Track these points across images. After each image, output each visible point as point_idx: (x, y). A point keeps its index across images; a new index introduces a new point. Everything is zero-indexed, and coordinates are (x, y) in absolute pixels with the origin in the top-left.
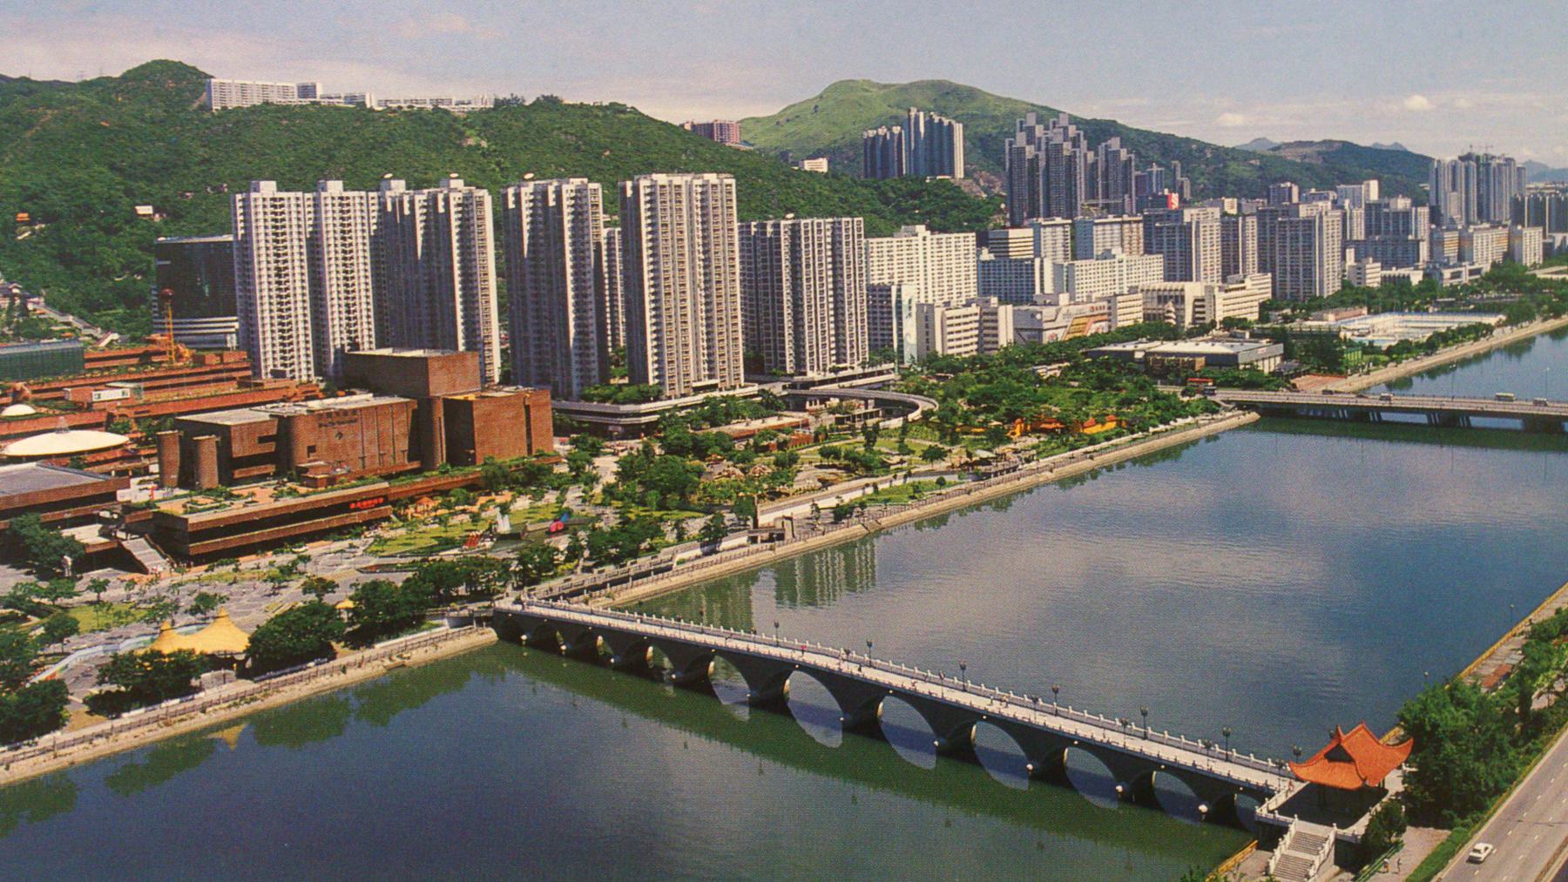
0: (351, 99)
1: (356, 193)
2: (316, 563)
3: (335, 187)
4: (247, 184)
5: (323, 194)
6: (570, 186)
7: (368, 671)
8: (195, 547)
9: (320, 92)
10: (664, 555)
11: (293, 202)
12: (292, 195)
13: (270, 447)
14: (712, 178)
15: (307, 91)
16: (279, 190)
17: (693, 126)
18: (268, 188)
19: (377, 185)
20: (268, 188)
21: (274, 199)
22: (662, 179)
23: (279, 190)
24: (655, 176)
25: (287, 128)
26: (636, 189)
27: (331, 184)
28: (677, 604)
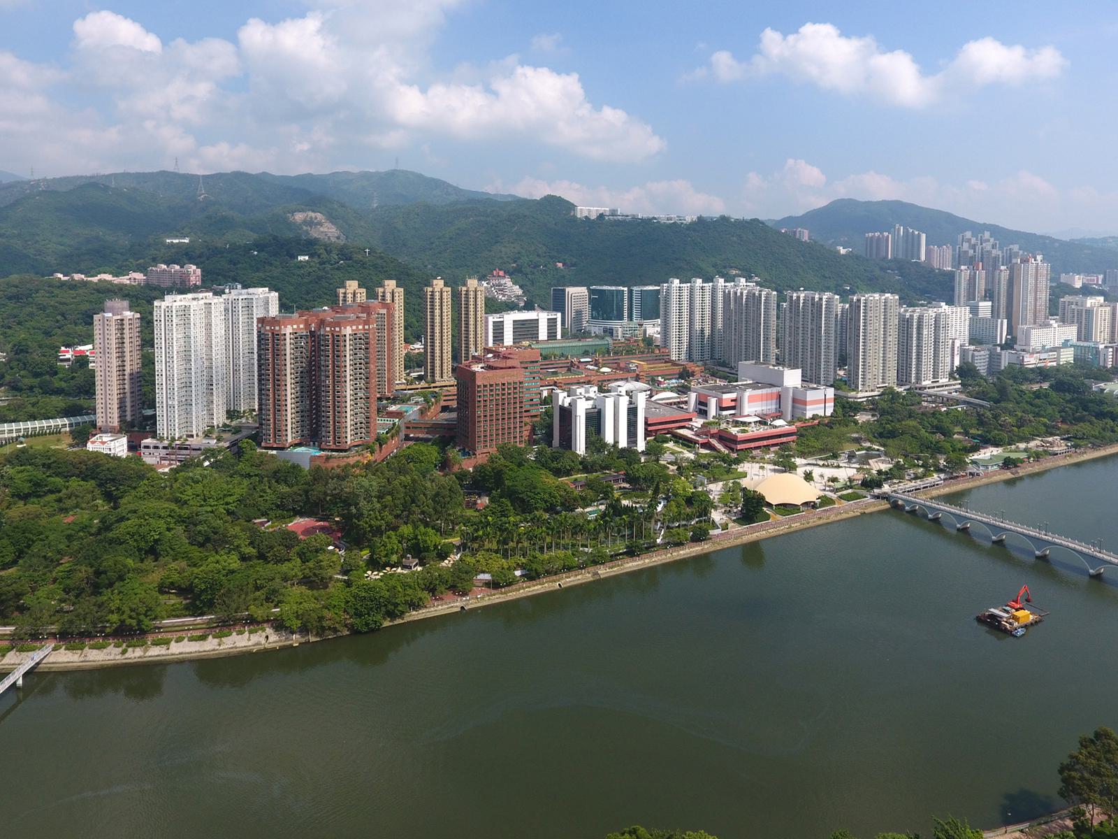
8: (739, 447)
26: (859, 300)
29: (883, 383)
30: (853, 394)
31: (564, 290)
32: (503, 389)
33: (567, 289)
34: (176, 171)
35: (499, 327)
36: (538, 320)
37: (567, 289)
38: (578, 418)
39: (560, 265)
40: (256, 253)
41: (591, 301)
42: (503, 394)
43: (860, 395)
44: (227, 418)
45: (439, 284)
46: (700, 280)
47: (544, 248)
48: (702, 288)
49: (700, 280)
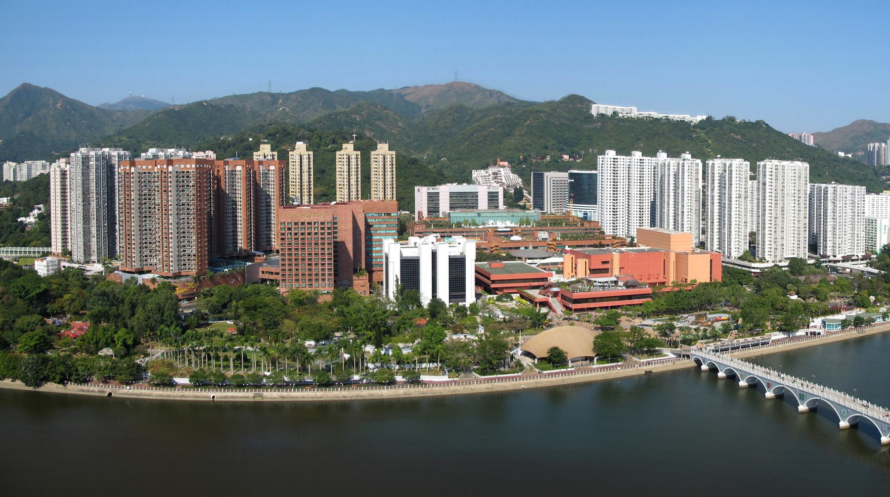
3: (638, 155)
20: (611, 154)
35: (433, 199)
37: (546, 174)
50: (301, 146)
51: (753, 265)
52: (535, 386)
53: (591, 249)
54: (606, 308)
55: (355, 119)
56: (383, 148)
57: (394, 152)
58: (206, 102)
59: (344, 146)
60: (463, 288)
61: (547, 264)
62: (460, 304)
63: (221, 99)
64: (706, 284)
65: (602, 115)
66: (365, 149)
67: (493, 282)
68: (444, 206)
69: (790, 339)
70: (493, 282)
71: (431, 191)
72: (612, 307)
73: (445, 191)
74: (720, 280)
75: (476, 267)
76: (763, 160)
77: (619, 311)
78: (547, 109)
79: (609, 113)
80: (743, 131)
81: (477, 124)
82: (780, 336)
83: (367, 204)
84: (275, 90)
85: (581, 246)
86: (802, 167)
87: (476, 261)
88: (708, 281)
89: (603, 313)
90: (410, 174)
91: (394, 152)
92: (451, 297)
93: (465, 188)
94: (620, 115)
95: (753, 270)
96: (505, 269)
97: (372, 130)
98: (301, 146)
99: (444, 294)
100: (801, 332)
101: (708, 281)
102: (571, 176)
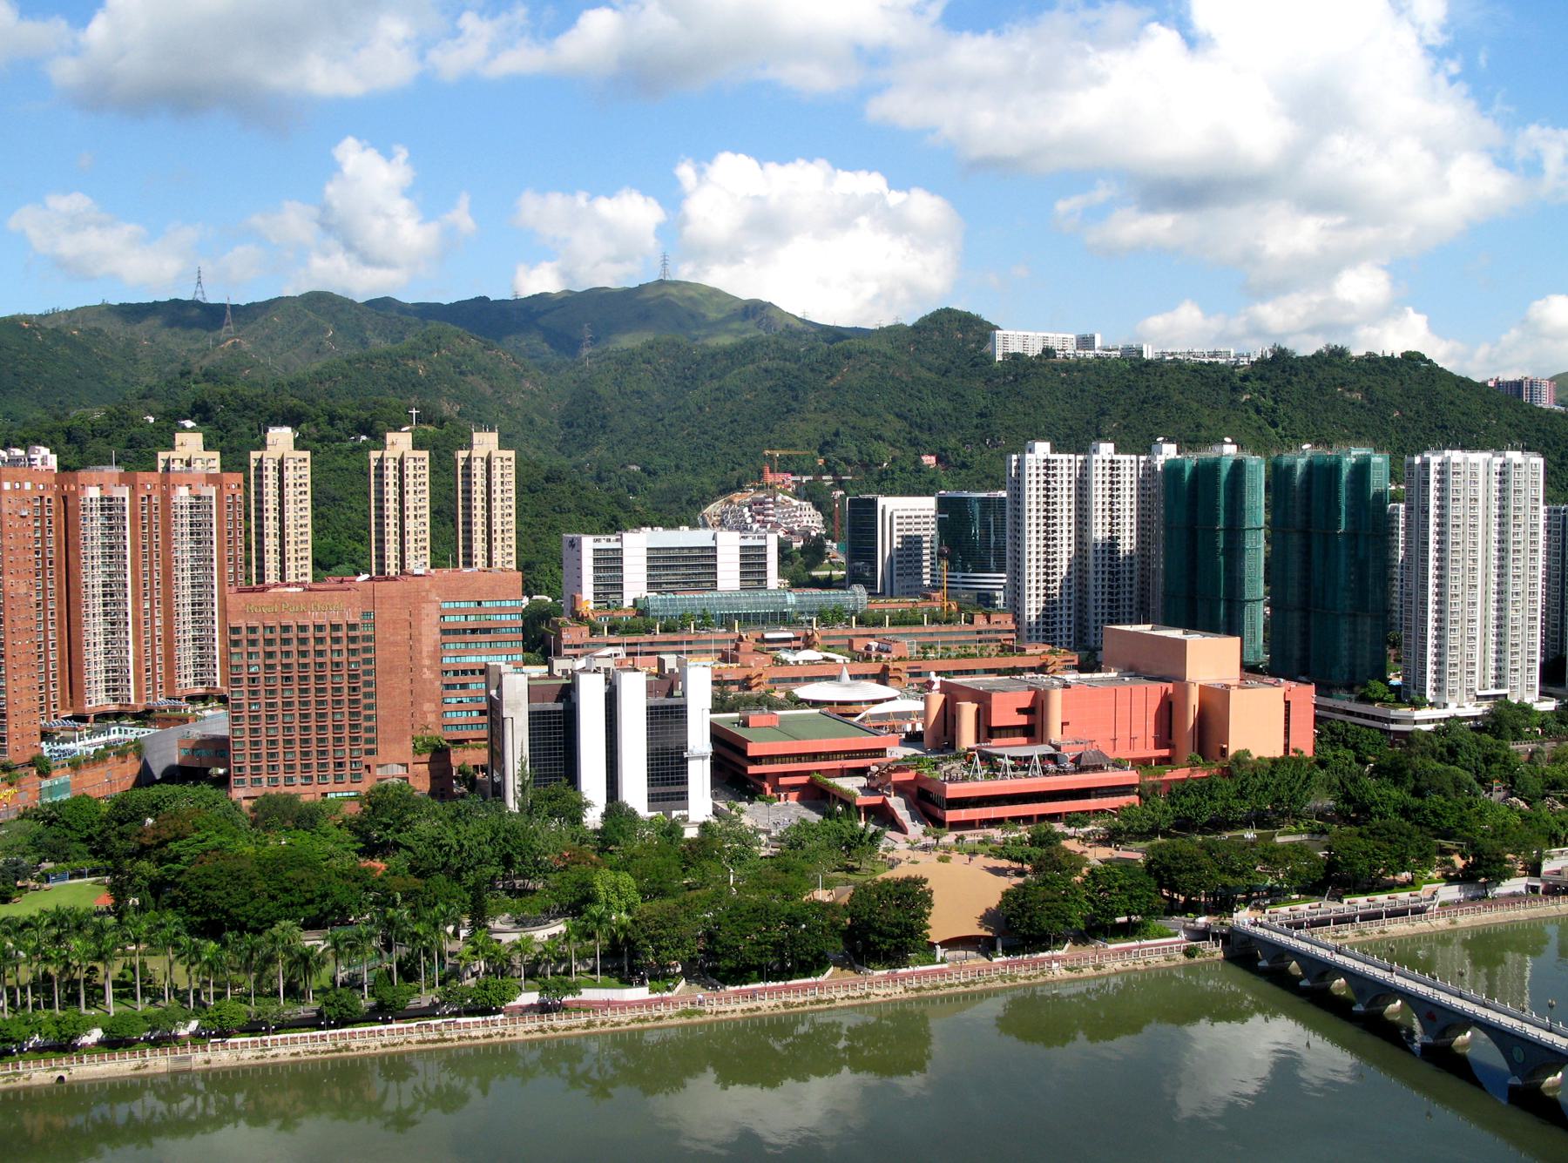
0: (1127, 350)
1: (1127, 457)
2: (1292, 875)
3: (1106, 450)
4: (1023, 448)
5: (1095, 457)
6: (1353, 455)
7: (897, 992)
8: (952, 815)
9: (1098, 343)
10: (1425, 891)
11: (1065, 464)
12: (1065, 457)
13: (1023, 720)
14: (1515, 456)
15: (1086, 342)
16: (1053, 451)
17: (1498, 383)
18: (1042, 449)
19: (1147, 448)
20: (1042, 449)
21: (1047, 461)
22: (1456, 456)
23: (1053, 451)
24: (1447, 453)
25: (1063, 382)
26: (1426, 465)
27: (1103, 446)
28: (1402, 954)
29: (1497, 686)
30: (1403, 711)
31: (874, 503)
32: (303, 641)
33: (882, 501)
34: (199, 297)
35: (610, 564)
36: (714, 549)
37: (882, 501)
38: (508, 724)
39: (929, 460)
40: (152, 420)
41: (942, 524)
42: (304, 654)
43: (1419, 714)
44: (849, 1029)
45: (400, 442)
46: (1110, 447)
47: (899, 425)
48: (1114, 466)
49: (1110, 447)
50: (281, 438)
51: (1394, 713)
52: (1547, 580)
53: (992, 678)
54: (1028, 819)
55: (415, 372)
56: (485, 442)
57: (511, 454)
58: (28, 318)
59: (391, 437)
60: (681, 777)
61: (886, 716)
62: (675, 814)
63: (70, 314)
64: (1274, 761)
65: (1016, 356)
66: (443, 448)
67: (757, 760)
68: (635, 584)
69: (1480, 898)
70: (757, 760)
71: (603, 545)
72: (1042, 818)
73: (636, 545)
74: (1309, 753)
75: (713, 726)
76: (1420, 452)
77: (1058, 827)
78: (886, 348)
79: (1034, 350)
80: (1365, 381)
81: (715, 384)
82: (1452, 892)
83: (446, 579)
84: (213, 298)
85: (967, 672)
86: (1530, 466)
87: (712, 711)
88: (1279, 753)
89: (1023, 832)
90: (558, 506)
91: (511, 454)
92: (653, 799)
93: (684, 537)
94: (1060, 355)
95: (1393, 727)
96: (785, 730)
97: (457, 400)
98: (281, 438)
99: (635, 793)
100: (1517, 884)
101: (1279, 753)
102: (943, 504)
